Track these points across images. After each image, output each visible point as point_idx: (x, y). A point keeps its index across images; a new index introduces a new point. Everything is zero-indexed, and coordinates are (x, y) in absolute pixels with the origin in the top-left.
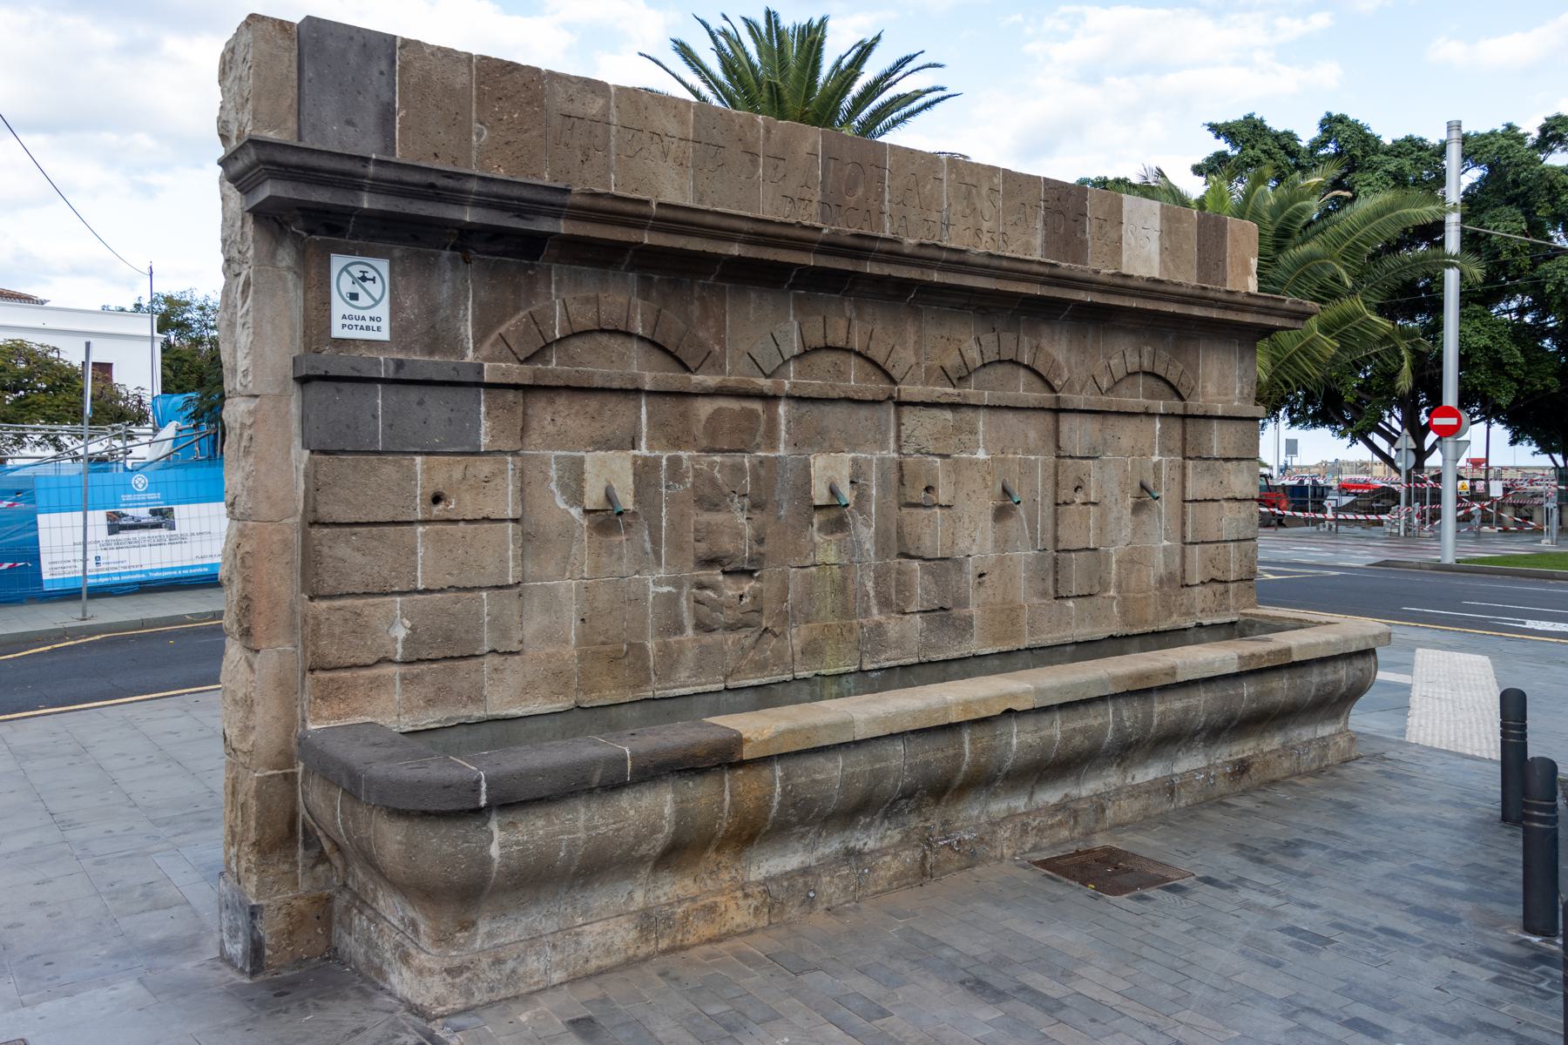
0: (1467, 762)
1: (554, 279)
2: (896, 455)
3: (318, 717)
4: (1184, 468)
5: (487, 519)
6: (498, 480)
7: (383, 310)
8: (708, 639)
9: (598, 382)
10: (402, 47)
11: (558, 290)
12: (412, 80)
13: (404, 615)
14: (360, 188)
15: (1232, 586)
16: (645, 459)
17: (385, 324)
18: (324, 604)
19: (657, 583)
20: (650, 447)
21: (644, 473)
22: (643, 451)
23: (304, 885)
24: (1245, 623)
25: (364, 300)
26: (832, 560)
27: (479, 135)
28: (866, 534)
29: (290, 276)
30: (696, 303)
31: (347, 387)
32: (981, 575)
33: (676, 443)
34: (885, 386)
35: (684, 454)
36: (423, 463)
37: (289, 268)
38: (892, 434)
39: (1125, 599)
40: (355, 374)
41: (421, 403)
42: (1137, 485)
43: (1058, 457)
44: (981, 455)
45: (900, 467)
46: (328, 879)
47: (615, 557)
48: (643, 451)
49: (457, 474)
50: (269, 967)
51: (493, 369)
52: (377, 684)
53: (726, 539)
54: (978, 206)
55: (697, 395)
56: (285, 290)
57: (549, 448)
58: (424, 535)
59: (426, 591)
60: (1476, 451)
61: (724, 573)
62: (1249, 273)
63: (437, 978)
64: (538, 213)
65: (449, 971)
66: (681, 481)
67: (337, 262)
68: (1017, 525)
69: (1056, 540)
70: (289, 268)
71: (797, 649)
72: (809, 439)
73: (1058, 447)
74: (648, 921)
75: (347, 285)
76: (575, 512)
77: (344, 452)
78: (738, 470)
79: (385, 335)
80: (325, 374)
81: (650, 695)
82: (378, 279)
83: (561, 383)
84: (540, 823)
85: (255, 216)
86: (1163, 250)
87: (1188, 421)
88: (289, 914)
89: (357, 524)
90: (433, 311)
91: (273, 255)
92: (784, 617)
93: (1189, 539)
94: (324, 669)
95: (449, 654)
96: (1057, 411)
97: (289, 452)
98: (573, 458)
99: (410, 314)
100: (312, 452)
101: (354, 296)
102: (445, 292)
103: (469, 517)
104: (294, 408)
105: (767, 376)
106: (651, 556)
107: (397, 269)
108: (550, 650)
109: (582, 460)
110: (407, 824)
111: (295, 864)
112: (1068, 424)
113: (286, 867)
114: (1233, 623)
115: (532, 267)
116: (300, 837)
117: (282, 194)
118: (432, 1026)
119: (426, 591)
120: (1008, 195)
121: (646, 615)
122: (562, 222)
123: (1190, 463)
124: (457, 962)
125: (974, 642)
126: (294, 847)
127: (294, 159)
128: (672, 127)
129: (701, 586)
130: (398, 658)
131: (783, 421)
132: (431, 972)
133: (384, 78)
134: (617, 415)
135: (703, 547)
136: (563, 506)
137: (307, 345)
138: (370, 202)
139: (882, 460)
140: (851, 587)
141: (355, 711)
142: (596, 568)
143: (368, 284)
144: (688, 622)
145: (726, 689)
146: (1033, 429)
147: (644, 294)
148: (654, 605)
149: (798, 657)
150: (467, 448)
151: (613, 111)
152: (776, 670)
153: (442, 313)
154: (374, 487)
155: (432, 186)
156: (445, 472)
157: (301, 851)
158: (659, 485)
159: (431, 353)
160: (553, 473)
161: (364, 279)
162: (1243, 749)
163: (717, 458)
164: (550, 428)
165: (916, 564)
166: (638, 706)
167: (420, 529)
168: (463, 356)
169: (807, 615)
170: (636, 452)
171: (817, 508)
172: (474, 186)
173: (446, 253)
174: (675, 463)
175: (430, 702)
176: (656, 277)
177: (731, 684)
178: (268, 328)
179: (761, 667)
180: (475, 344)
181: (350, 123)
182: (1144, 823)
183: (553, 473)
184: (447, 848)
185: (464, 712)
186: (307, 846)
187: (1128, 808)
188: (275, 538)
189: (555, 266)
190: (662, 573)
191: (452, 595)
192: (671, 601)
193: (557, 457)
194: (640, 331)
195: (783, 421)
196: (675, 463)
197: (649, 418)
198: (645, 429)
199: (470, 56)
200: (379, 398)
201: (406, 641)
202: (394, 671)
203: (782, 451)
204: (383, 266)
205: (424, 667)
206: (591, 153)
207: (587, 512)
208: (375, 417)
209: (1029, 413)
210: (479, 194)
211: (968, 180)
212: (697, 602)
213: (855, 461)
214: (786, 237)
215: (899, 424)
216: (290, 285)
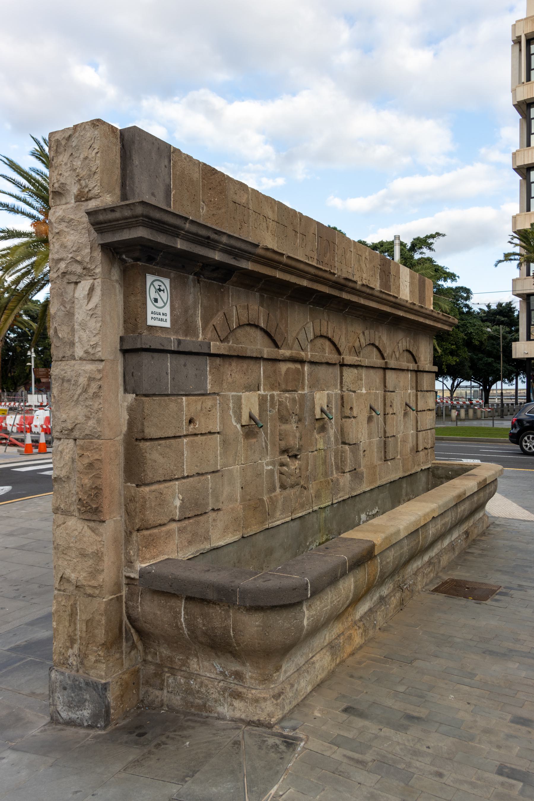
0: (527, 523)
1: (230, 294)
2: (339, 392)
3: (143, 560)
4: (417, 396)
5: (210, 433)
7: (167, 309)
9: (249, 354)
10: (173, 152)
11: (232, 301)
12: (178, 173)
13: (180, 492)
14: (177, 236)
15: (429, 450)
17: (168, 318)
18: (147, 489)
19: (267, 465)
20: (264, 390)
21: (262, 400)
22: (262, 392)
23: (126, 664)
24: (434, 467)
25: (160, 303)
26: (322, 447)
27: (203, 208)
29: (117, 286)
30: (279, 310)
31: (156, 355)
33: (272, 388)
34: (336, 356)
35: (275, 393)
36: (186, 401)
37: (117, 281)
38: (339, 381)
39: (403, 459)
40: (162, 348)
41: (185, 365)
42: (405, 404)
43: (385, 391)
44: (364, 391)
45: (342, 398)
46: (136, 659)
47: (253, 451)
48: (262, 392)
50: (113, 720)
51: (215, 345)
55: (280, 361)
56: (115, 295)
58: (187, 443)
59: (188, 477)
61: (290, 457)
62: (431, 305)
63: (268, 702)
64: (242, 257)
65: (274, 697)
66: (274, 408)
67: (150, 278)
68: (373, 425)
69: (385, 432)
70: (117, 281)
71: (313, 495)
72: (315, 385)
73: (385, 386)
74: (332, 647)
76: (239, 426)
77: (154, 395)
79: (168, 325)
80: (136, 347)
81: (267, 526)
82: (165, 290)
83: (235, 354)
84: (318, 603)
85: (102, 247)
86: (411, 291)
87: (418, 373)
88: (121, 685)
89: (160, 439)
90: (186, 311)
91: (110, 272)
92: (307, 478)
93: (419, 430)
94: (147, 529)
95: (197, 513)
96: (385, 369)
97: (118, 395)
98: (238, 396)
99: (178, 312)
100: (137, 395)
102: (191, 300)
103: (203, 432)
104: (120, 369)
106: (265, 449)
107: (172, 285)
108: (231, 506)
109: (241, 396)
110: (262, 614)
111: (122, 653)
112: (390, 374)
113: (117, 656)
114: (429, 468)
115: (222, 287)
116: (124, 635)
117: (146, 236)
118: (274, 730)
122: (250, 263)
123: (419, 393)
124: (276, 691)
125: (364, 485)
126: (121, 642)
127: (157, 215)
128: (270, 214)
129: (282, 465)
130: (177, 518)
131: (306, 375)
132: (265, 699)
133: (167, 169)
135: (283, 443)
136: (235, 424)
137: (126, 329)
138: (181, 245)
139: (336, 394)
140: (327, 461)
141: (162, 553)
142: (246, 458)
143: (162, 292)
144: (278, 485)
145: (292, 520)
146: (376, 376)
147: (261, 304)
149: (314, 499)
151: (250, 202)
152: (308, 507)
153: (190, 312)
154: (165, 416)
155: (208, 238)
157: (124, 644)
159: (186, 336)
161: (160, 290)
162: (465, 527)
163: (287, 395)
164: (230, 380)
165: (347, 447)
166: (262, 533)
167: (185, 440)
168: (198, 337)
169: (315, 476)
170: (259, 392)
171: (317, 420)
172: (224, 239)
173: (191, 277)
174: (272, 396)
176: (265, 295)
177: (294, 516)
178: (108, 318)
179: (302, 506)
180: (203, 330)
182: (452, 565)
184: (287, 625)
186: (127, 640)
187: (445, 560)
188: (112, 450)
189: (231, 287)
191: (196, 478)
192: (271, 472)
193: (232, 396)
194: (262, 325)
195: (306, 375)
196: (272, 396)
197: (264, 373)
198: (262, 380)
199: (199, 163)
200: (169, 361)
201: (181, 507)
202: (174, 526)
204: (167, 282)
205: (187, 522)
207: (242, 426)
208: (167, 374)
209: (377, 370)
210: (225, 244)
212: (281, 473)
213: (328, 394)
214: (324, 278)
215: (342, 376)
216: (117, 291)
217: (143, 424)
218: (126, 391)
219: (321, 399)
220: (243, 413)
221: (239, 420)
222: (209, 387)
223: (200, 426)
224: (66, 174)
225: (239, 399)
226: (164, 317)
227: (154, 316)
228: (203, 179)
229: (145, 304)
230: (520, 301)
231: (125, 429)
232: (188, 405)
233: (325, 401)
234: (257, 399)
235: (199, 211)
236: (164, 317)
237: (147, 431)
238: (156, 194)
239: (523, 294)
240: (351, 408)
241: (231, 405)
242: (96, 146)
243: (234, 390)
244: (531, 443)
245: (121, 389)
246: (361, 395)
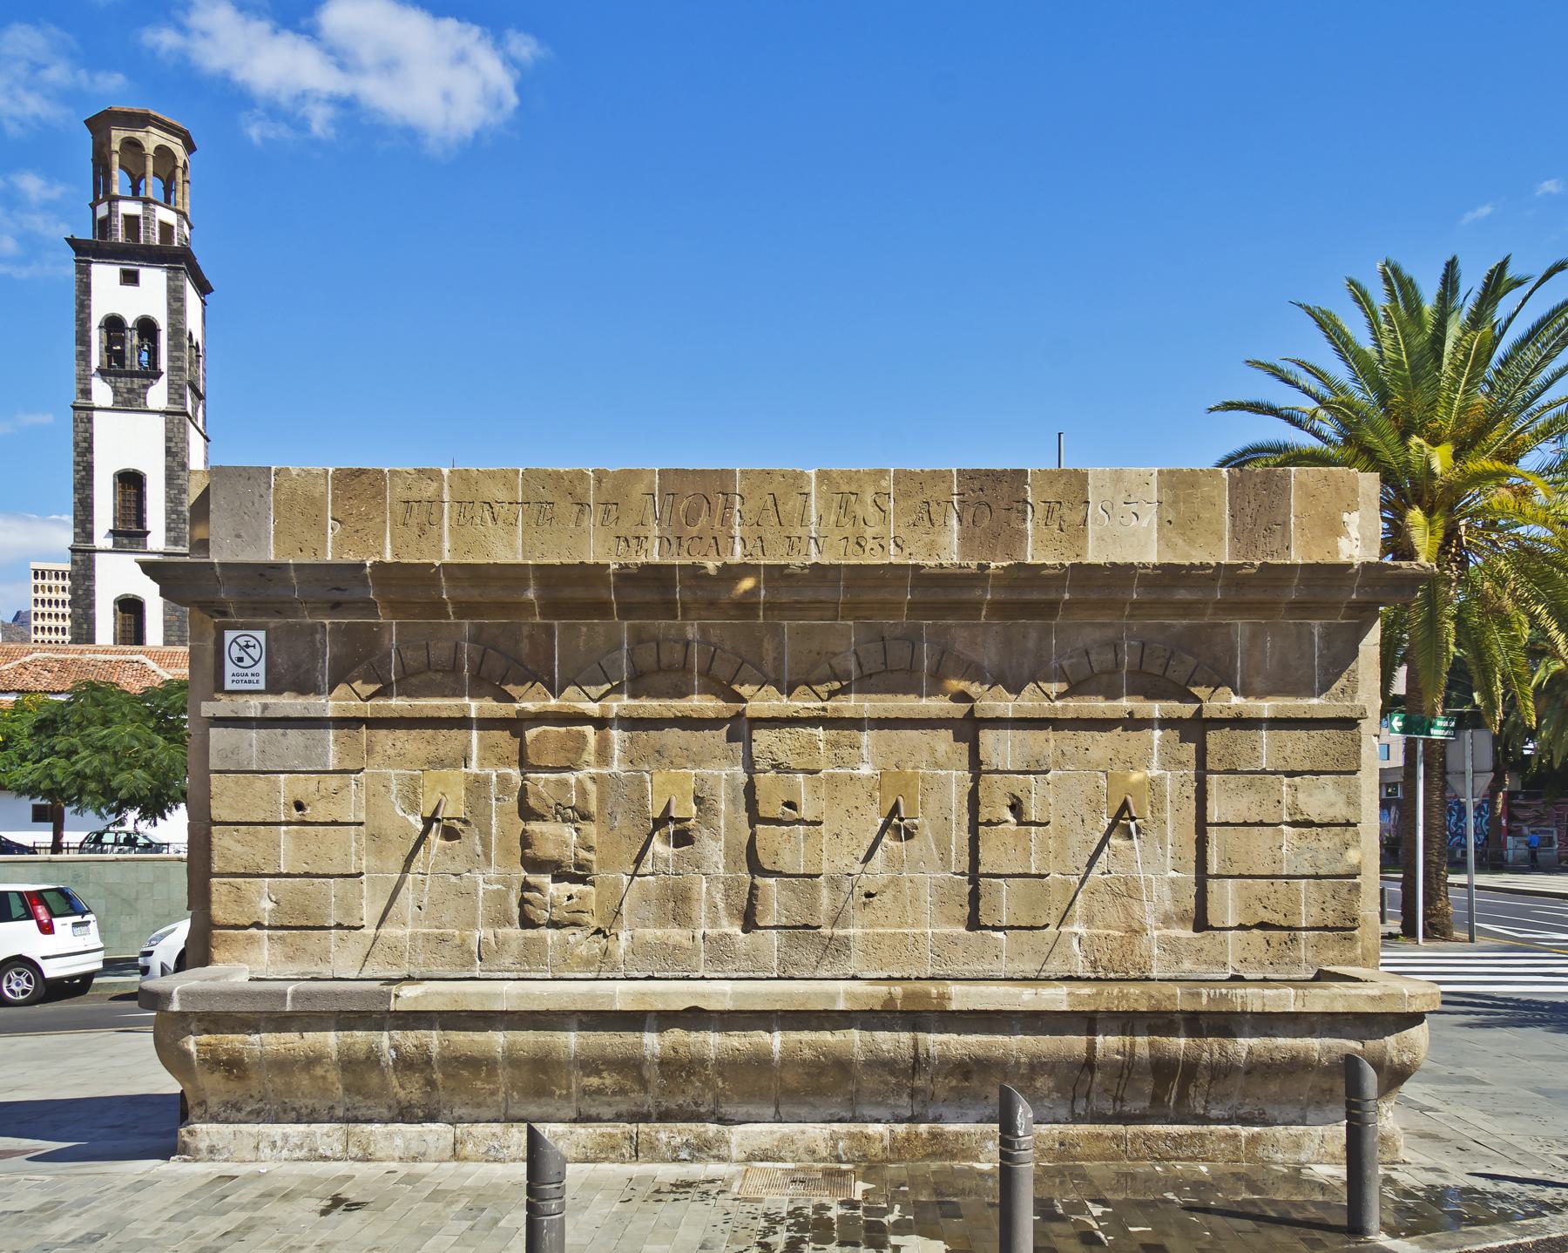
5: (335, 823)
6: (344, 792)
8: (529, 933)
16: (477, 775)
22: (474, 768)
25: (248, 662)
28: (714, 850)
32: (869, 895)
44: (866, 770)
48: (474, 768)
49: (312, 787)
52: (251, 940)
53: (551, 845)
54: (860, 514)
57: (390, 766)
60: (129, 827)
75: (236, 652)
78: (564, 784)
101: (241, 659)
105: (595, 701)
112: (987, 737)
119: (288, 875)
120: (903, 495)
121: (476, 909)
134: (449, 741)
136: (401, 814)
148: (485, 900)
150: (319, 768)
156: (303, 787)
158: (488, 798)
160: (394, 788)
167: (284, 828)
175: (291, 959)
181: (239, 536)
183: (394, 788)
185: (315, 969)
190: (492, 873)
192: (501, 897)
203: (616, 767)
206: (427, 527)
211: (845, 488)
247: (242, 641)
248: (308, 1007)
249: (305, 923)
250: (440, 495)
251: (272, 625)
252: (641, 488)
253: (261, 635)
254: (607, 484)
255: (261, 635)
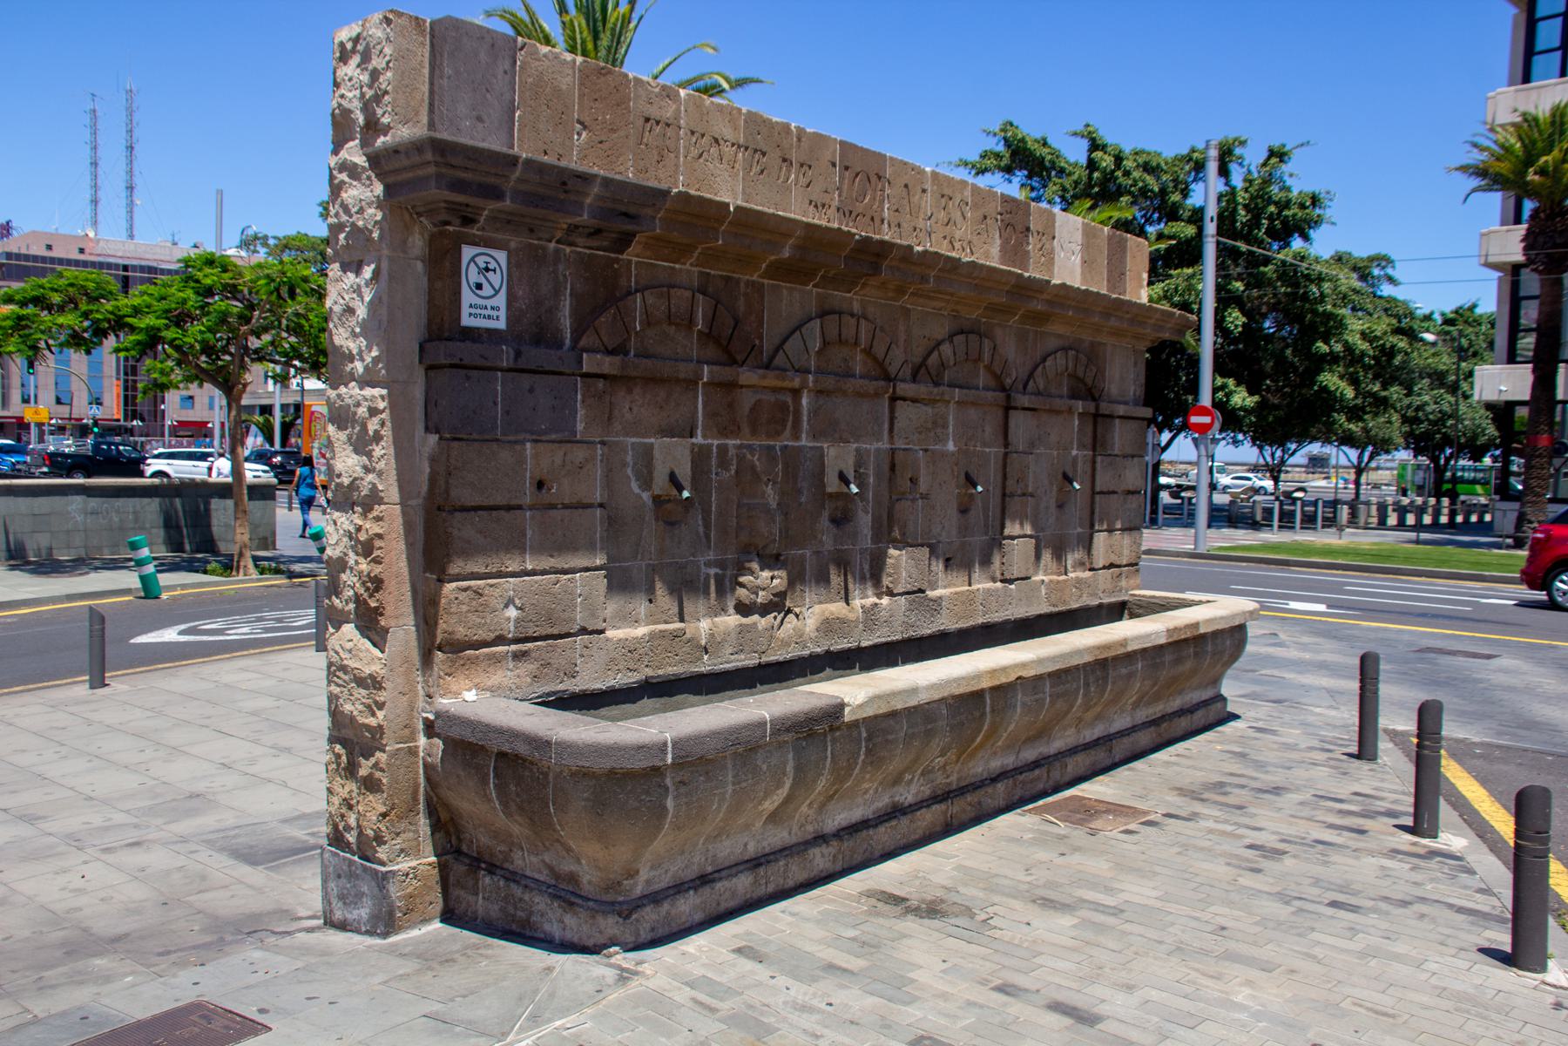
4: (1094, 462)
7: (501, 300)
16: (701, 447)
17: (503, 314)
20: (704, 437)
21: (700, 457)
22: (699, 439)
25: (487, 291)
33: (724, 432)
38: (886, 426)
41: (531, 391)
48: (699, 439)
66: (728, 469)
128: (727, 132)
131: (805, 412)
139: (878, 450)
161: (487, 269)
181: (479, 119)
195: (805, 412)
196: (723, 450)
197: (704, 407)
208: (495, 403)
213: (857, 450)
217: (447, 482)
218: (427, 429)
219: (839, 457)
220: (656, 474)
221: (646, 483)
222: (580, 427)
223: (562, 490)
224: (350, 95)
225: (647, 454)
226: (495, 313)
227: (473, 311)
228: (581, 84)
229: (457, 293)
230: (1500, 279)
231: (425, 488)
232: (536, 456)
233: (851, 461)
234: (687, 452)
235: (571, 138)
236: (495, 313)
237: (454, 493)
238: (485, 117)
239: (1505, 264)
240: (913, 481)
241: (629, 459)
242: (388, 51)
243: (636, 435)
244: (1565, 584)
245: (421, 427)
246: (944, 455)
247: (481, 261)
248: (1175, 638)
249: (550, 631)
250: (677, 118)
251: (513, 245)
252: (828, 156)
253: (502, 256)
254: (805, 144)
255: (502, 256)
